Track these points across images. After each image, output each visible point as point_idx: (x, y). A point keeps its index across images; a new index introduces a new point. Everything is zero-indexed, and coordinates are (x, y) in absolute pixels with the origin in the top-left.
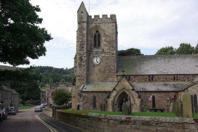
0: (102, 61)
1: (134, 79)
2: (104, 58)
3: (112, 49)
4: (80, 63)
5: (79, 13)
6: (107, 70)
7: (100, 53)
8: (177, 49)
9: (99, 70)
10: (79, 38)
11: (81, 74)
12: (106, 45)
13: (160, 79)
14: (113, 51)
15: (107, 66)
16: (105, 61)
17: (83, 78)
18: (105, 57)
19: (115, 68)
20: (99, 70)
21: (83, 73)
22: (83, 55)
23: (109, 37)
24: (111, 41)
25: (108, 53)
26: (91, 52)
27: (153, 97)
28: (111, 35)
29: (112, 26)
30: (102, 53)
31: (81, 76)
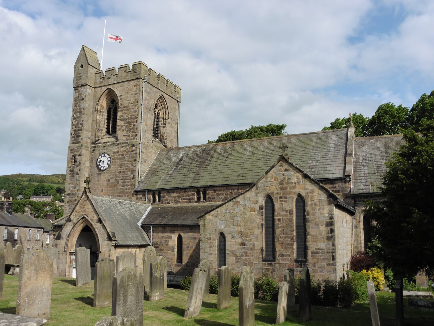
0: (113, 161)
1: (166, 197)
2: (117, 154)
3: (131, 134)
4: (72, 169)
5: (77, 69)
6: (122, 180)
7: (111, 144)
8: (370, 117)
9: (106, 181)
10: (74, 119)
11: (72, 191)
12: (122, 126)
13: (218, 195)
14: (134, 139)
15: (120, 172)
16: (119, 162)
17: (74, 199)
18: (118, 152)
19: (134, 176)
20: (106, 181)
21: (75, 188)
22: (78, 151)
23: (128, 110)
24: (131, 118)
25: (125, 145)
26: (98, 143)
27: (180, 238)
28: (132, 105)
29: (134, 86)
30: (114, 144)
31: (73, 194)
